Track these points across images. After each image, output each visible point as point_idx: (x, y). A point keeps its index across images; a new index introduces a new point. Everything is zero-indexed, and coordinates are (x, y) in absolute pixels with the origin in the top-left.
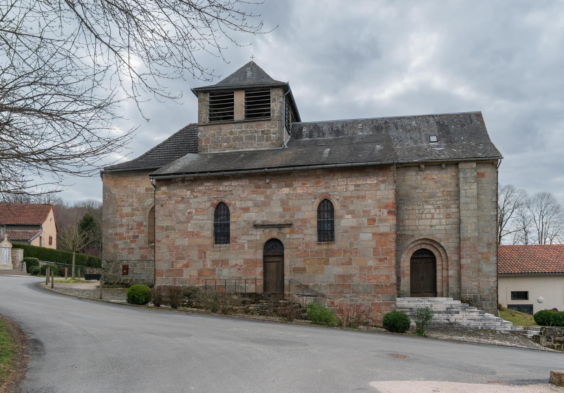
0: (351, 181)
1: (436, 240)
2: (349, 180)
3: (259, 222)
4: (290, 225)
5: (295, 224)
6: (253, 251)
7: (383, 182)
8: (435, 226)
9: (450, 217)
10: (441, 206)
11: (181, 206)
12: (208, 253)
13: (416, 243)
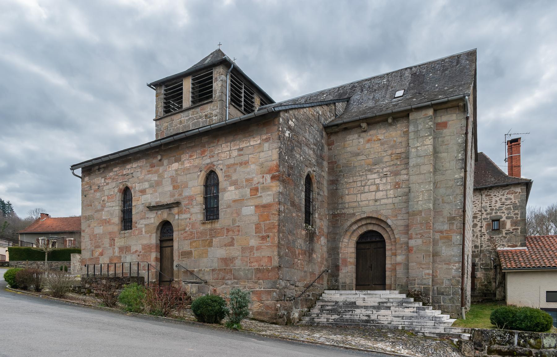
0: (235, 145)
1: (382, 218)
2: (232, 144)
3: (153, 204)
4: (177, 204)
5: (184, 203)
6: (148, 235)
7: (267, 140)
8: (380, 200)
9: (399, 187)
10: (389, 173)
11: (98, 194)
12: (116, 239)
13: (360, 224)
